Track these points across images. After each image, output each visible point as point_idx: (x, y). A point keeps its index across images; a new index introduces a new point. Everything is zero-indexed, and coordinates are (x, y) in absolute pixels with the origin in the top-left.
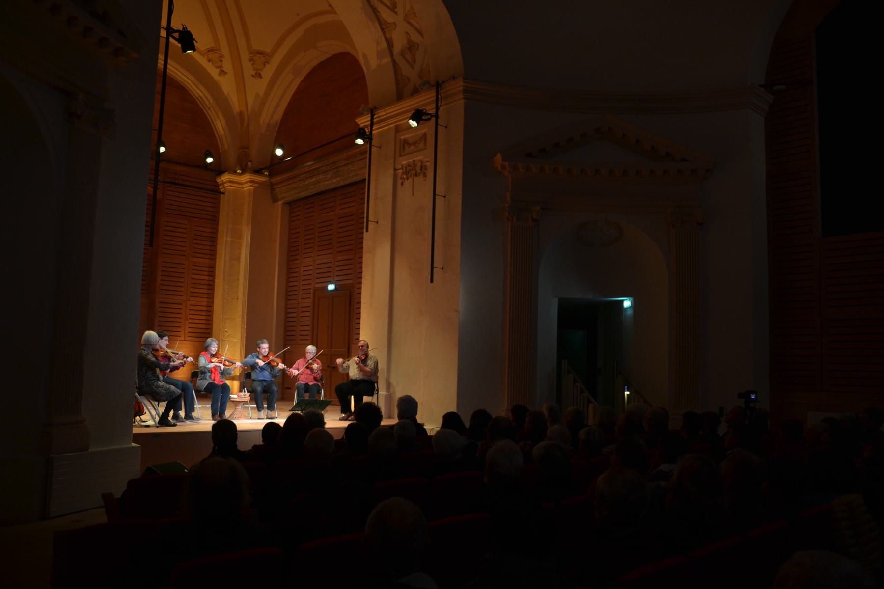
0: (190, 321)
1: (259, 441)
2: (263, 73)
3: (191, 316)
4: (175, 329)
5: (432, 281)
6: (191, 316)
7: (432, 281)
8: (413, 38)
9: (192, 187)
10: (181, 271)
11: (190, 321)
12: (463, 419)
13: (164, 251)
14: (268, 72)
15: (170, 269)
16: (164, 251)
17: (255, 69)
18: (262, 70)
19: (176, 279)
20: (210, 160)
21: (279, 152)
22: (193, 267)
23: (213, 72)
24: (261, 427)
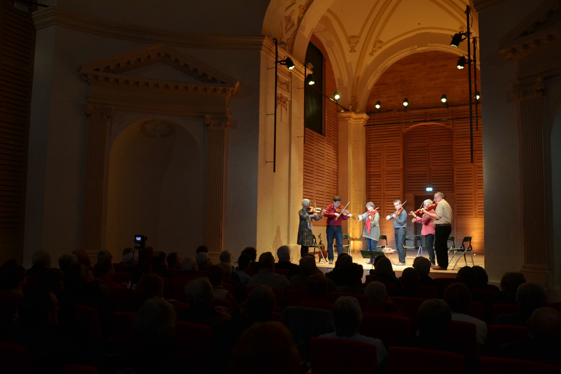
0: (479, 204)
1: (455, 277)
2: (355, 49)
3: (479, 201)
4: (469, 210)
5: (274, 171)
6: (479, 201)
7: (274, 171)
8: (292, 17)
9: (465, 118)
10: (470, 172)
11: (479, 204)
12: (257, 253)
13: (457, 162)
14: (359, 47)
15: (462, 173)
16: (457, 162)
17: (351, 47)
18: (355, 47)
19: (467, 178)
20: (444, 100)
21: (337, 97)
22: (478, 169)
23: (369, 50)
24: (403, 270)
